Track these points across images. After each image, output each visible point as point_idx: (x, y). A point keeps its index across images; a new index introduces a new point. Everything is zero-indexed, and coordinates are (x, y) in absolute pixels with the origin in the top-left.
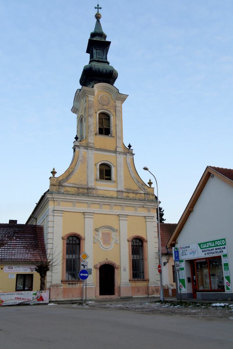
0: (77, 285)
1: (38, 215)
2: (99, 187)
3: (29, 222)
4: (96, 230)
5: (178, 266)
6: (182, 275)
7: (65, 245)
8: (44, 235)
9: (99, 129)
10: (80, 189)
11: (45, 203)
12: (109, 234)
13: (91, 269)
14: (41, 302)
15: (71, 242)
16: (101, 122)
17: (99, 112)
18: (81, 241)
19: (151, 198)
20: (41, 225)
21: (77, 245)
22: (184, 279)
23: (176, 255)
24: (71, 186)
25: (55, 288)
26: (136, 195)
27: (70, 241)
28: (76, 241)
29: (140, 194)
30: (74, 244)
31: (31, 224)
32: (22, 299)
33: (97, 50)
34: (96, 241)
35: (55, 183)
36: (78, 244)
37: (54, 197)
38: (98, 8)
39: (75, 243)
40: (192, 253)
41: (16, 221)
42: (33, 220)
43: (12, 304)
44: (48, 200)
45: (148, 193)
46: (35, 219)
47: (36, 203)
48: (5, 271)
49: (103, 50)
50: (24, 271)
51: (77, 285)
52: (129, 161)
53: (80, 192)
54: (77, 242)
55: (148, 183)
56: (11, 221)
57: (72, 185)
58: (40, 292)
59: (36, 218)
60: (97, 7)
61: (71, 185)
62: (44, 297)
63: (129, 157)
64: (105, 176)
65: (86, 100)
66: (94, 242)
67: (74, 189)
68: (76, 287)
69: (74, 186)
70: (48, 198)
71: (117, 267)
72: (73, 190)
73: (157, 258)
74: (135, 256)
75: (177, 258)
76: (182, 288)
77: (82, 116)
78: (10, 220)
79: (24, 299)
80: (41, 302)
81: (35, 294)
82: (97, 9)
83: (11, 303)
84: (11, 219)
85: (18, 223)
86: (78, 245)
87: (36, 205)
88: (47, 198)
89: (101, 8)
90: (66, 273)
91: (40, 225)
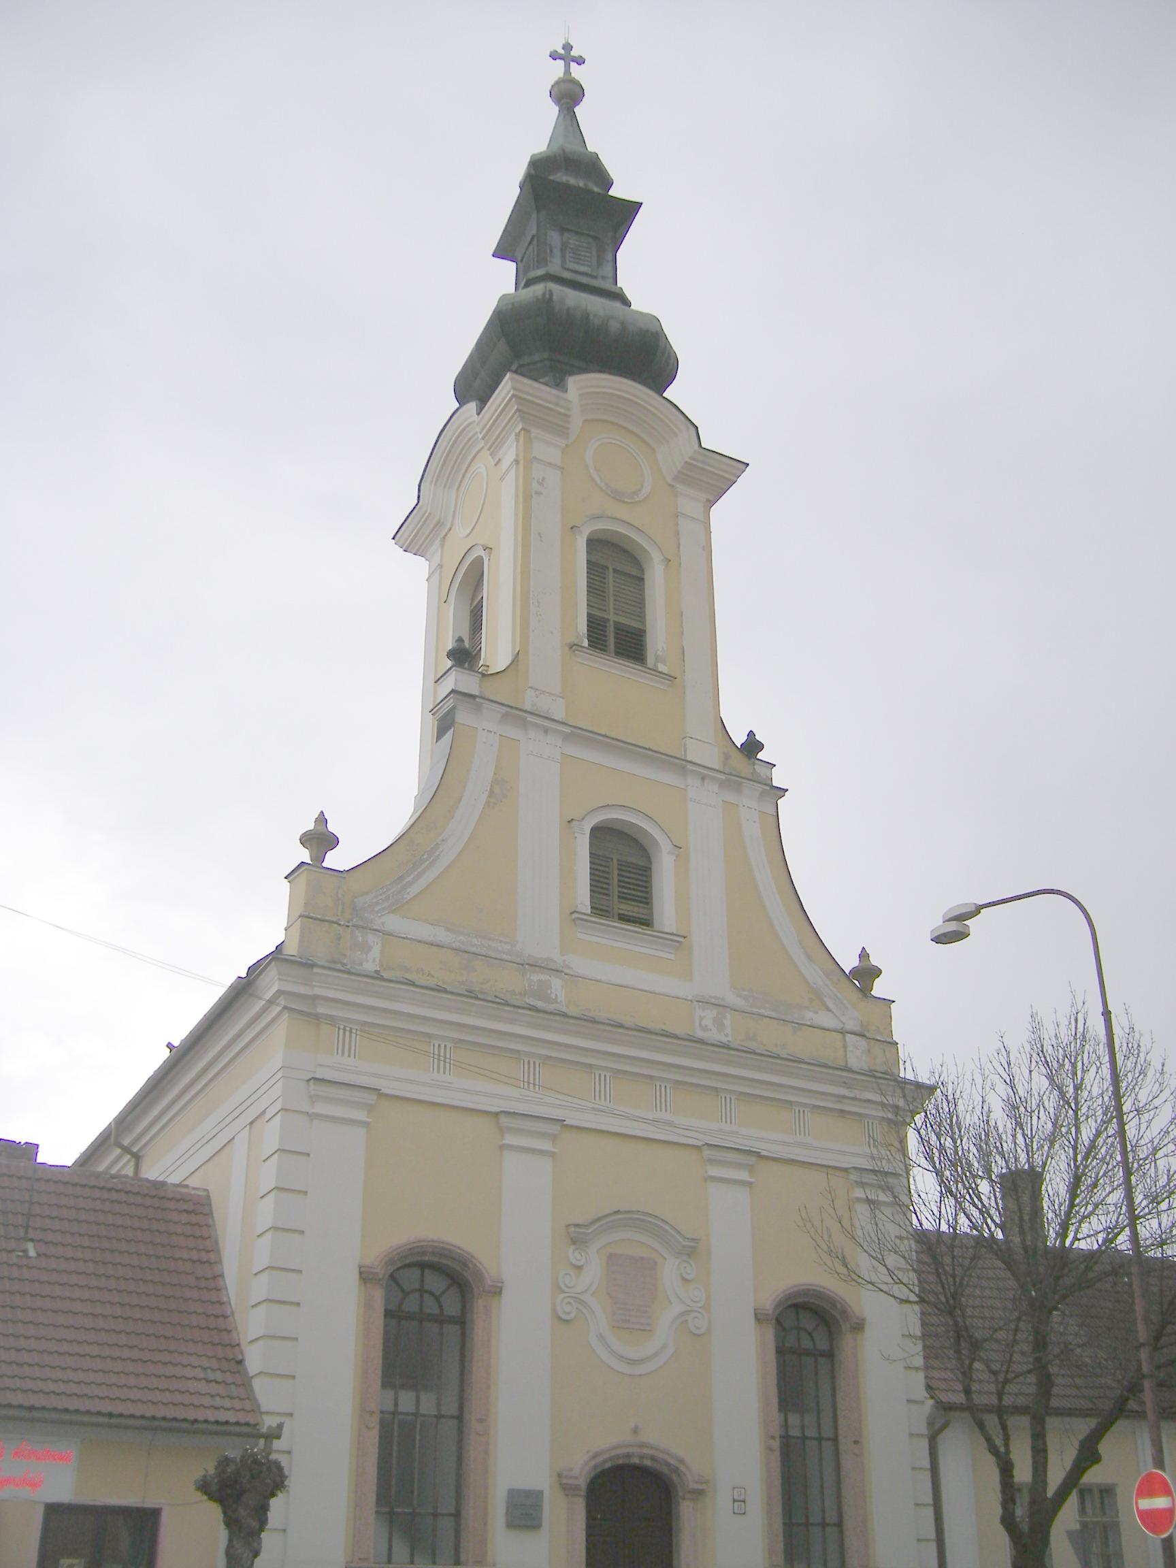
1: (154, 1130)
2: (580, 965)
4: (577, 1236)
7: (379, 1322)
8: (216, 1249)
9: (592, 620)
11: (239, 1036)
12: (647, 1267)
13: (540, 1494)
15: (411, 1304)
18: (479, 1304)
27: (406, 1294)
28: (443, 1300)
33: (566, 235)
34: (568, 1308)
36: (452, 1320)
37: (318, 991)
38: (566, 55)
39: (437, 1311)
41: (32, 1148)
47: (169, 1046)
49: (595, 238)
52: (752, 828)
59: (135, 1149)
63: (749, 803)
66: (554, 1310)
71: (692, 1485)
73: (918, 1435)
74: (794, 1419)
82: (561, 63)
86: (452, 1330)
87: (166, 1053)
89: (580, 61)
90: (377, 1512)
91: (180, 1185)
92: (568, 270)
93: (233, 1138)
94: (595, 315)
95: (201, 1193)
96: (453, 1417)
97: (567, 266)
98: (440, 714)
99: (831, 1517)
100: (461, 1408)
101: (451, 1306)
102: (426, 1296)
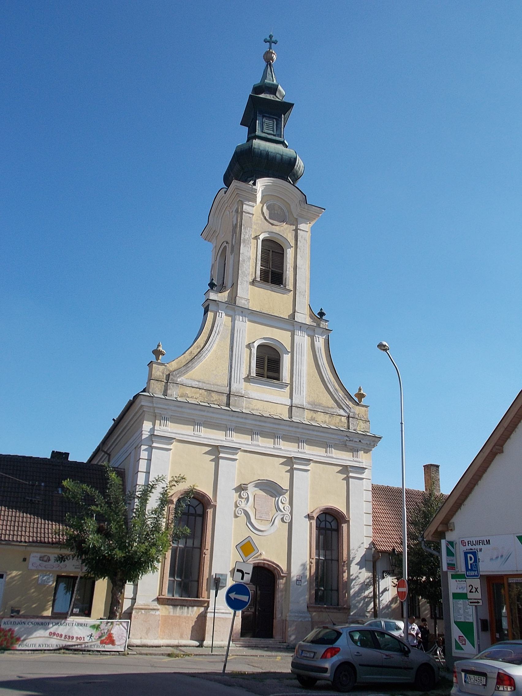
0: (192, 612)
1: (113, 446)
2: (253, 394)
3: (95, 459)
5: (474, 590)
6: (464, 612)
10: (213, 394)
11: (120, 434)
14: (109, 647)
16: (265, 260)
17: (262, 237)
19: (362, 427)
20: (119, 467)
21: (197, 518)
22: (472, 623)
23: (470, 562)
24: (194, 386)
25: (142, 613)
26: (330, 417)
28: (196, 508)
29: (340, 417)
30: (192, 515)
31: (99, 464)
32: (66, 636)
35: (160, 376)
36: (199, 515)
38: (270, 41)
40: (497, 558)
41: (67, 454)
42: (103, 455)
43: (40, 648)
44: (141, 411)
45: (357, 416)
46: (106, 455)
47: (114, 420)
48: (30, 567)
50: (75, 568)
51: (192, 612)
53: (212, 399)
54: (199, 511)
55: (356, 395)
56: (55, 454)
57: (197, 383)
58: (109, 624)
60: (269, 39)
61: (195, 384)
62: (115, 637)
64: (268, 370)
65: (237, 209)
67: (201, 391)
68: (189, 615)
69: (200, 385)
70: (142, 406)
72: (198, 395)
75: (471, 570)
76: (465, 644)
77: (225, 244)
78: (53, 452)
79: (69, 637)
80: (109, 647)
81: (97, 627)
83: (39, 645)
84: (56, 450)
85: (70, 459)
88: (140, 405)
89: (275, 43)
92: (265, 133)
93: (131, 453)
94: (271, 152)
95: (122, 470)
96: (198, 548)
97: (264, 131)
98: (205, 306)
99: (335, 587)
100: (201, 545)
101: (199, 511)
102: (327, 522)
